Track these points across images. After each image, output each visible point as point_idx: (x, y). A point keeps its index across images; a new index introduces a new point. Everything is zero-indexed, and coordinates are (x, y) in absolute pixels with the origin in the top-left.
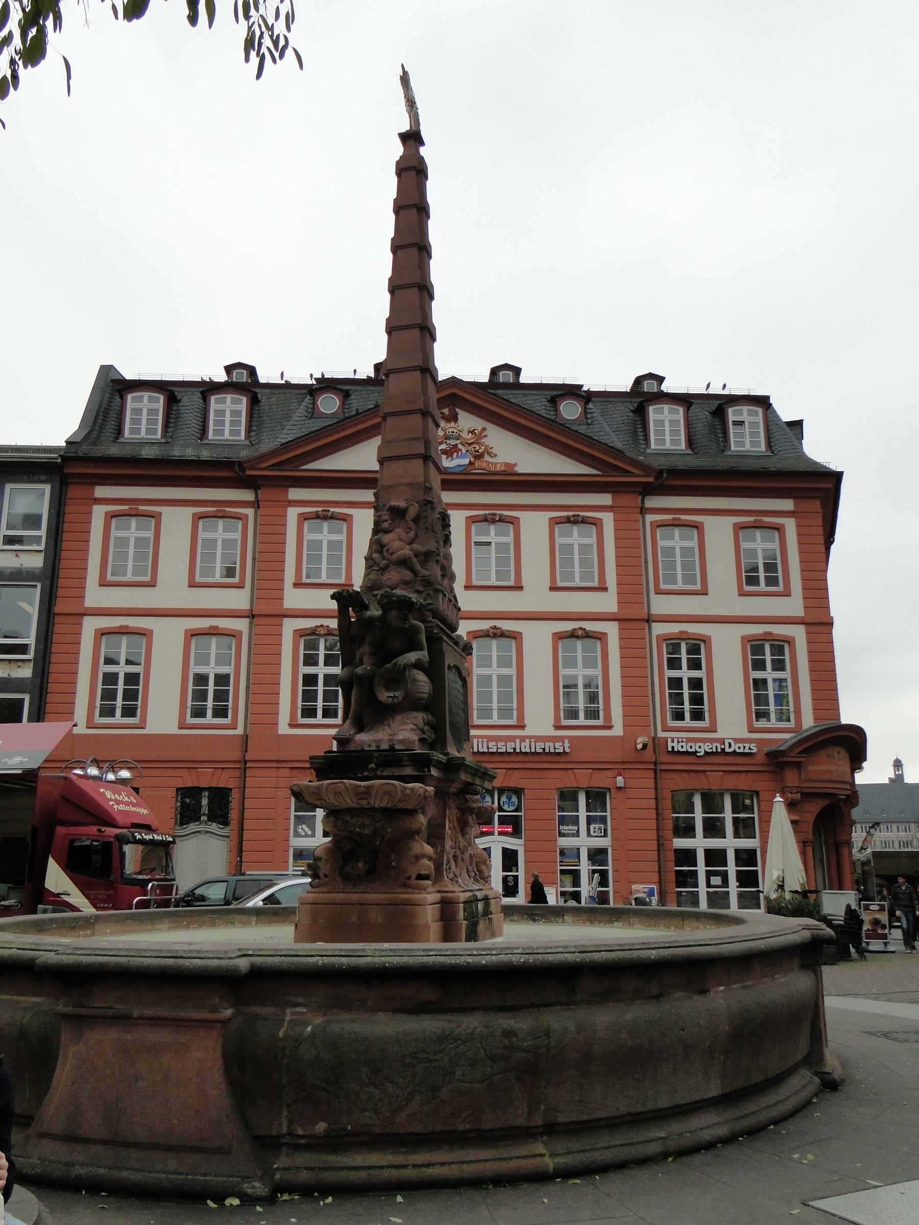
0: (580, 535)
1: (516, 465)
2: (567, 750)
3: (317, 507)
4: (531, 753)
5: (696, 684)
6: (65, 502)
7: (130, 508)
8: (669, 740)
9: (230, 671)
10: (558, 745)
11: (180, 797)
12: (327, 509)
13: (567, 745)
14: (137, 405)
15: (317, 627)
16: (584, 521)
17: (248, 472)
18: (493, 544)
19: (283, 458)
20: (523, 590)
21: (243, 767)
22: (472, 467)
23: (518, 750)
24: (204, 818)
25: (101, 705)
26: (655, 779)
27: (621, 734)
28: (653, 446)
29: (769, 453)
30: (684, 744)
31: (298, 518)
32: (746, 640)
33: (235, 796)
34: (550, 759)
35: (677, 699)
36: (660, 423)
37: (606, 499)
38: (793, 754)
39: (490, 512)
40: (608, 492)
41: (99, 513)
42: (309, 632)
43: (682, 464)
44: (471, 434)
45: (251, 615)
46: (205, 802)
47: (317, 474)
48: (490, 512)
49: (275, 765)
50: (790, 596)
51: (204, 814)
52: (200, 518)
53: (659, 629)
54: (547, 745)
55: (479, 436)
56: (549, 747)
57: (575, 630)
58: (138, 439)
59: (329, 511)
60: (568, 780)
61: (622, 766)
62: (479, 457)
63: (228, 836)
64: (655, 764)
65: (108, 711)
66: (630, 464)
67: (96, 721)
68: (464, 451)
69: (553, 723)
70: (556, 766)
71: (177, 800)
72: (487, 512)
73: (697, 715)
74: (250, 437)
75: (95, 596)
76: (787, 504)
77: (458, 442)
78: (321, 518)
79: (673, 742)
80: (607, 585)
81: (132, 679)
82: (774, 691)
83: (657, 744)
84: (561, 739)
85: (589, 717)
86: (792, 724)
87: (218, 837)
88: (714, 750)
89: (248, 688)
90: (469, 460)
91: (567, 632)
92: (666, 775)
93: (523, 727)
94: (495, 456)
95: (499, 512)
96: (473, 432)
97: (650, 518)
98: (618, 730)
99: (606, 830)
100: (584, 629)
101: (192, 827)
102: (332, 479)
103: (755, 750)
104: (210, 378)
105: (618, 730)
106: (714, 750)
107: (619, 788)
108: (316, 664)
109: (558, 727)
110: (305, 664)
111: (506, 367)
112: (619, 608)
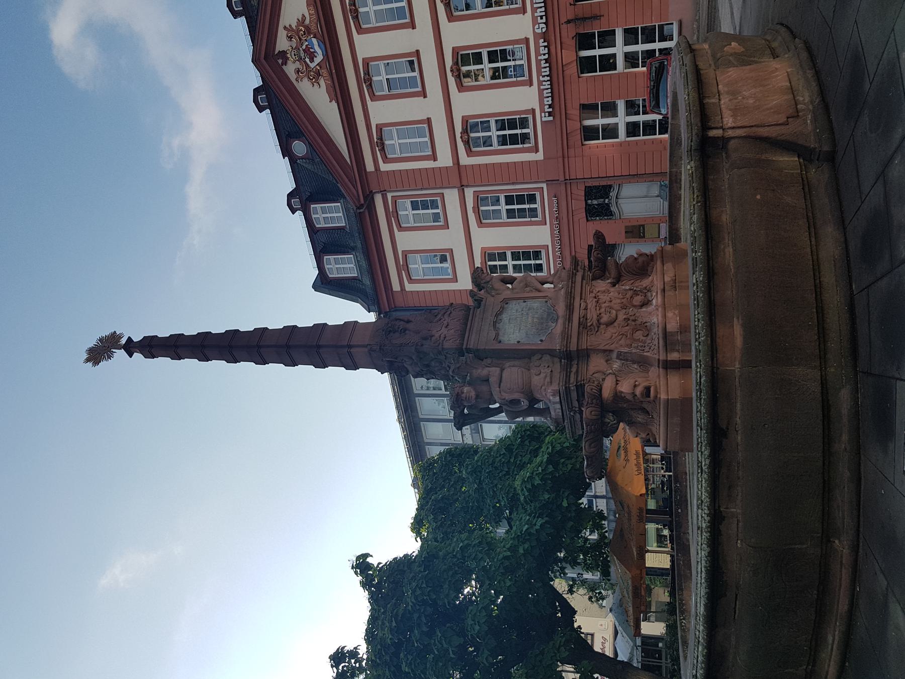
3: (376, 151)
5: (515, 256)
6: (407, 307)
7: (403, 270)
9: (493, 120)
11: (592, 218)
12: (376, 144)
15: (462, 141)
16: (367, 73)
17: (362, 201)
18: (388, 77)
19: (347, 180)
20: (430, 118)
21: (569, 181)
22: (318, 36)
24: (607, 201)
25: (521, 144)
33: (590, 183)
41: (409, 287)
42: (467, 146)
44: (293, 39)
45: (462, 188)
46: (595, 202)
49: (566, 160)
50: (452, 250)
51: (604, 201)
53: (465, 160)
58: (344, 218)
59: (377, 142)
63: (619, 185)
68: (307, 43)
69: (528, 87)
72: (350, 17)
75: (445, 159)
77: (301, 49)
78: (383, 147)
80: (426, 118)
81: (501, 125)
85: (535, 213)
87: (620, 191)
88: (544, 13)
89: (513, 184)
90: (312, 39)
91: (465, 147)
92: (597, 490)
93: (533, 111)
94: (303, 15)
95: (348, 7)
101: (613, 208)
104: (284, 158)
106: (549, 83)
108: (506, 266)
109: (524, 11)
111: (256, 101)
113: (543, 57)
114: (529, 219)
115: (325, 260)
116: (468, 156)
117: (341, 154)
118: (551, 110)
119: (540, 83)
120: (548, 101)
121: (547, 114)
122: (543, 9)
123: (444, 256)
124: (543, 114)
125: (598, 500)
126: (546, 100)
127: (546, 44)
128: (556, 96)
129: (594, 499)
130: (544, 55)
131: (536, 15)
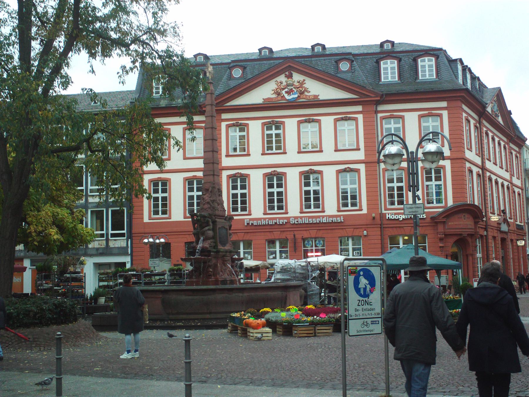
0: (433, 122)
1: (319, 95)
2: (342, 221)
4: (302, 224)
8: (387, 214)
10: (338, 219)
13: (342, 218)
14: (385, 66)
16: (313, 121)
23: (321, 222)
26: (381, 231)
27: (366, 213)
28: (383, 80)
29: (437, 80)
30: (393, 216)
31: (298, 123)
32: (186, 179)
34: (335, 225)
35: (391, 196)
36: (423, 67)
37: (359, 108)
38: (441, 218)
39: (308, 118)
40: (445, 101)
43: (398, 88)
47: (235, 107)
48: (308, 118)
50: (170, 160)
52: (383, 119)
54: (334, 219)
55: (302, 83)
56: (335, 220)
57: (346, 168)
60: (270, 237)
61: (366, 226)
62: (302, 93)
64: (381, 225)
65: (156, 213)
66: (369, 92)
67: (152, 217)
68: (295, 91)
70: (339, 227)
71: (185, 247)
72: (306, 118)
73: (280, 208)
74: (438, 76)
75: (226, 162)
76: (444, 104)
79: (388, 215)
82: (436, 190)
83: (383, 216)
84: (339, 216)
86: (443, 204)
88: (299, 223)
92: (387, 229)
93: (250, 215)
95: (311, 118)
96: (299, 82)
97: (380, 115)
98: (365, 211)
99: (361, 253)
100: (350, 168)
102: (342, 103)
103: (425, 217)
105: (365, 211)
107: (365, 236)
108: (273, 187)
109: (339, 211)
110: (305, 186)
112: (365, 157)
113: (278, 221)
114: (152, 210)
115: (394, 61)
116: (227, 176)
117: (231, 101)
118: (250, 224)
119: (265, 219)
120: (255, 223)
121: (248, 222)
122: (301, 223)
123: (245, 151)
124: (248, 220)
125: (126, 241)
126: (256, 222)
127: (284, 223)
128: (257, 228)
129: (125, 238)
130: (279, 222)
131: (299, 219)
